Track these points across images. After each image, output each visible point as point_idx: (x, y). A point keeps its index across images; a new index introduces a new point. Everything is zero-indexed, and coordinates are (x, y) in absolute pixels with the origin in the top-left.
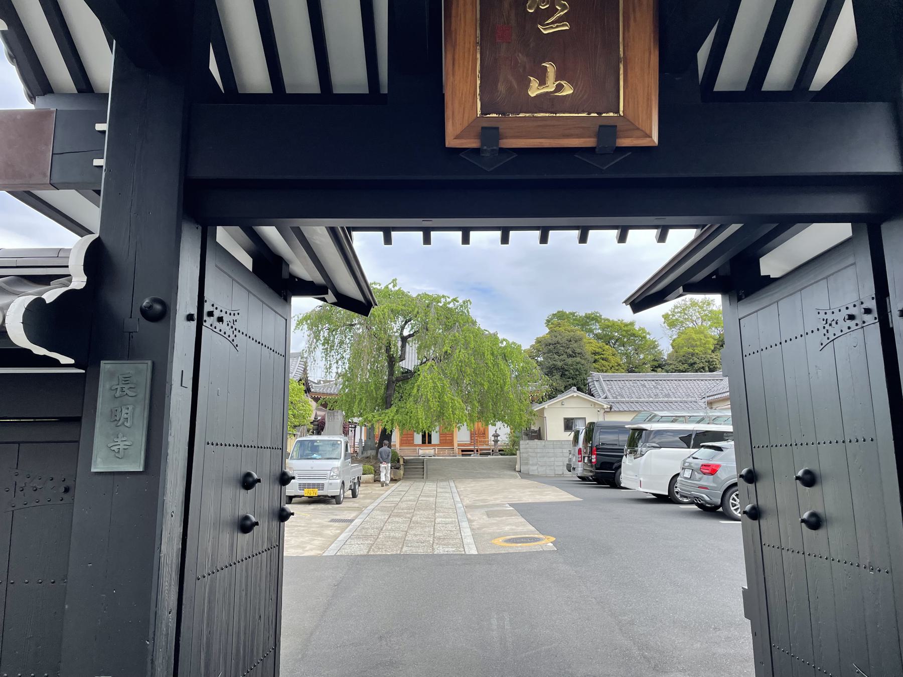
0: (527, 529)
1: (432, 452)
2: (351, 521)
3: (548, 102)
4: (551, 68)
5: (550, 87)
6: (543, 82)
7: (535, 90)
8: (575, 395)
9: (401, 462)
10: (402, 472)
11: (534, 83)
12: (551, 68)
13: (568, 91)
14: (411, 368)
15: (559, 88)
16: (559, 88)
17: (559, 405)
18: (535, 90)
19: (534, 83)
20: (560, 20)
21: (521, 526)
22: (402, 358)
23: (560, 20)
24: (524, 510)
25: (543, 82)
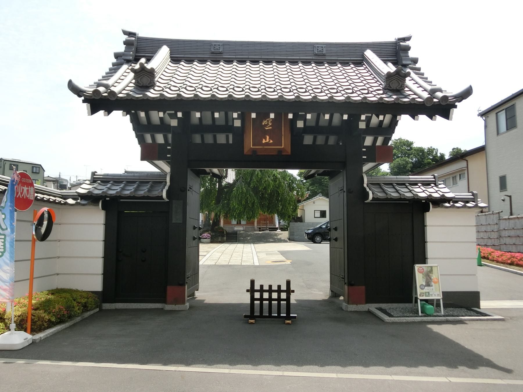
0: (283, 258)
1: (241, 229)
2: (205, 256)
3: (267, 144)
4: (268, 137)
5: (268, 141)
6: (266, 140)
7: (264, 141)
8: (321, 198)
9: (225, 233)
10: (225, 238)
11: (264, 140)
12: (268, 137)
13: (271, 141)
14: (231, 182)
15: (269, 141)
16: (269, 141)
17: (312, 203)
18: (264, 141)
19: (264, 140)
20: (270, 126)
21: (281, 258)
22: (226, 176)
23: (270, 126)
24: (283, 253)
25: (266, 140)
